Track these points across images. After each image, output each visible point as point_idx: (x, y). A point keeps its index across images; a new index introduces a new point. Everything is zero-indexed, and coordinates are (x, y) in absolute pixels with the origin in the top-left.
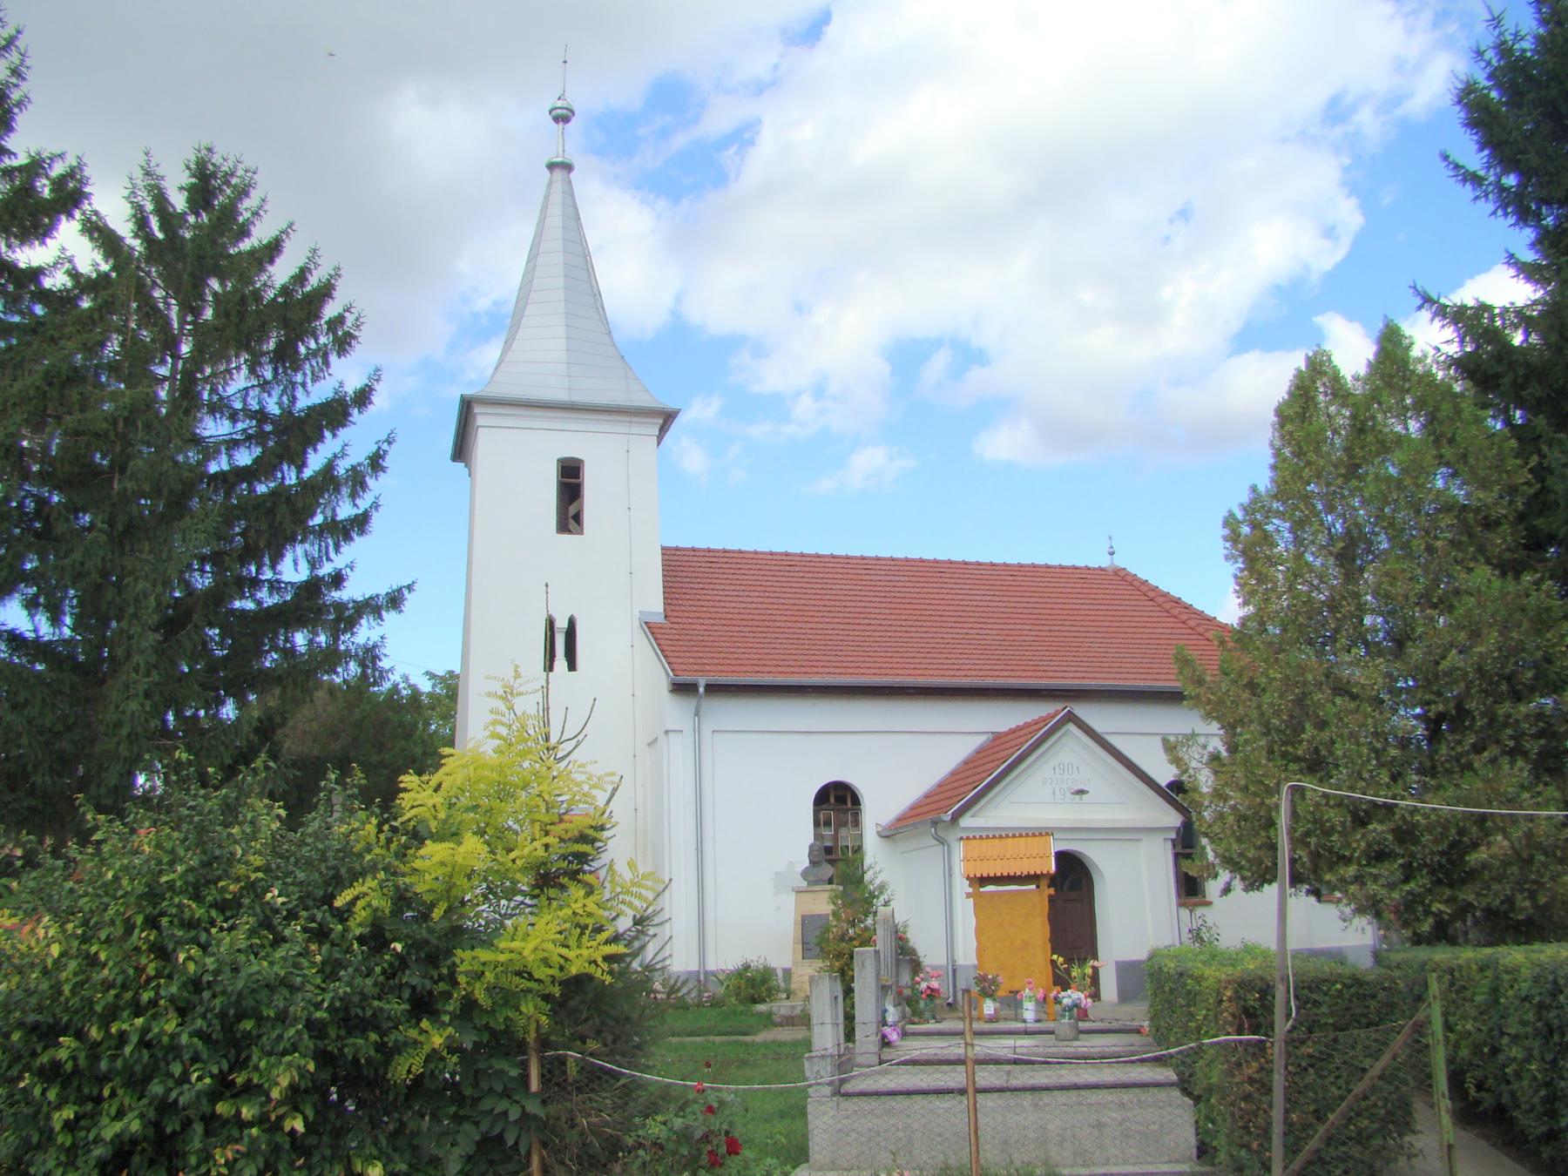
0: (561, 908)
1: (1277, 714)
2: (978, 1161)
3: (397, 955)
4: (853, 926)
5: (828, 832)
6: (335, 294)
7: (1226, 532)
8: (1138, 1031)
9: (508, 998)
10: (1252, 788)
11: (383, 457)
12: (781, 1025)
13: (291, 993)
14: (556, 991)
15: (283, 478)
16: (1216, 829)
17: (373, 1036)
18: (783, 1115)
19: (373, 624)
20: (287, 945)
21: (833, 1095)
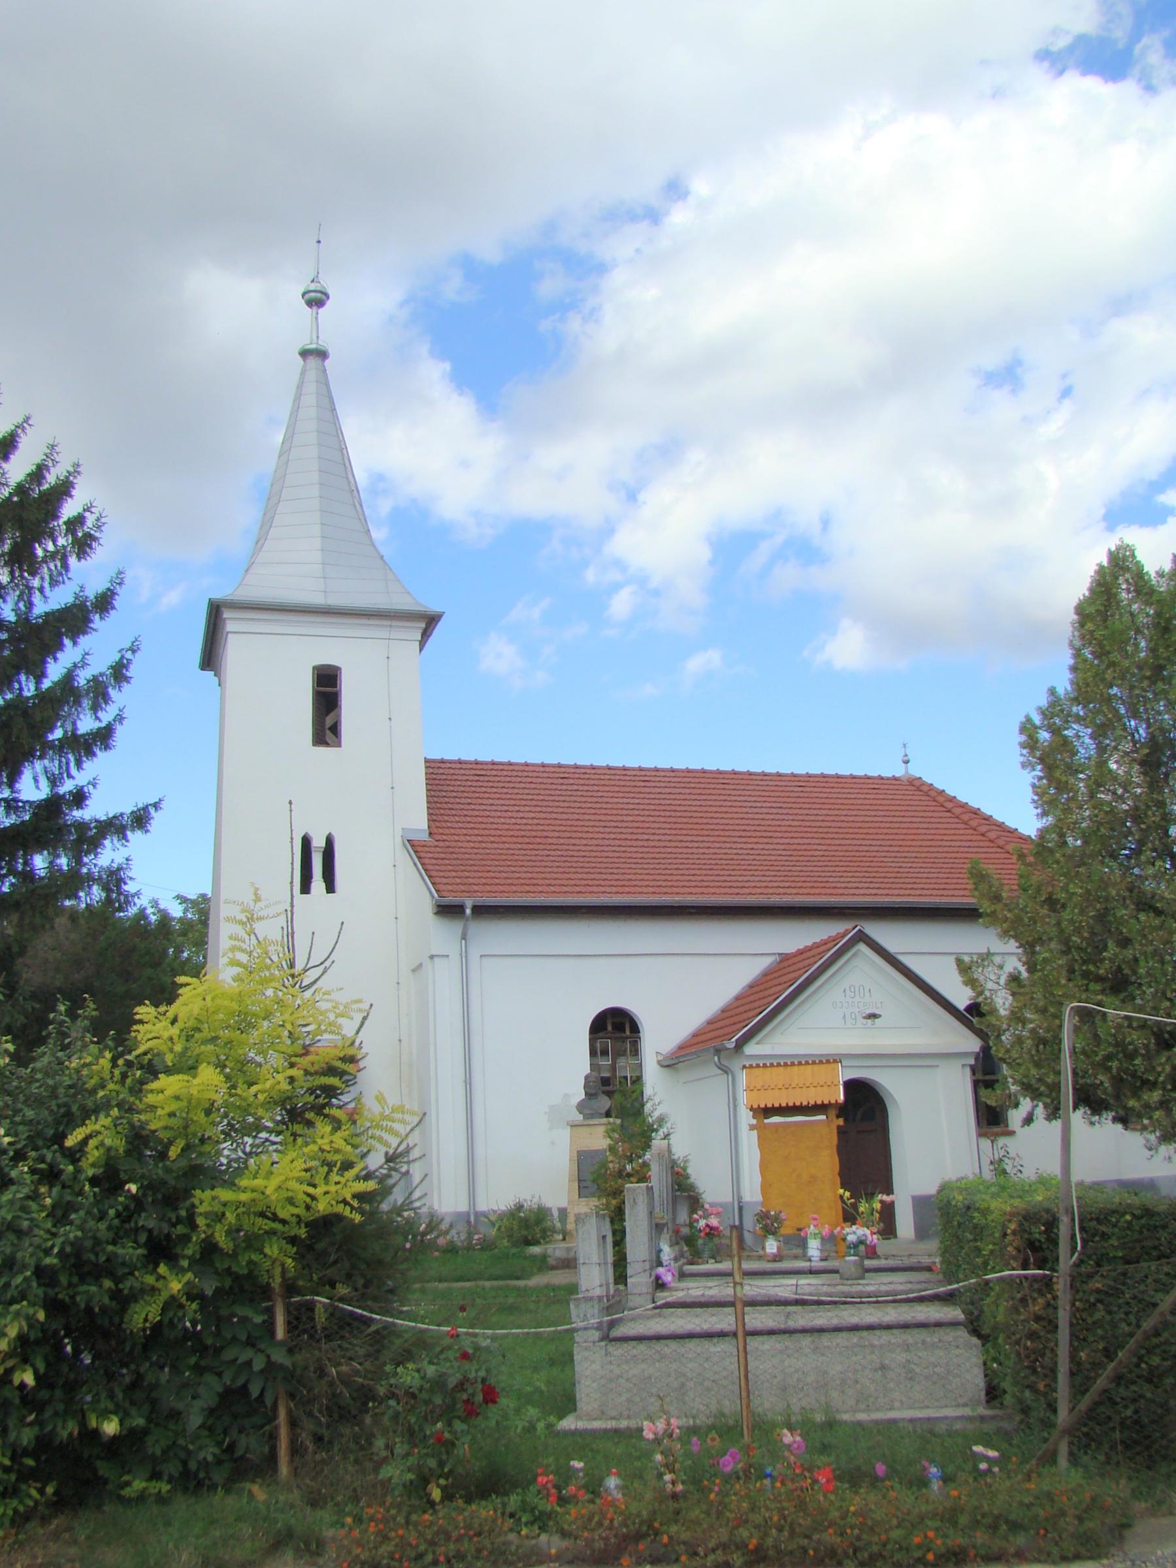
0: (307, 1144)
1: (1078, 930)
2: (748, 1406)
3: (134, 1197)
4: (631, 1161)
5: (606, 1062)
6: (74, 493)
7: (1023, 738)
8: (929, 1269)
9: (253, 1242)
10: (1052, 1010)
11: (126, 667)
12: (553, 1268)
13: (19, 1238)
14: (302, 1232)
15: (21, 689)
16: (1014, 1055)
17: (108, 1283)
18: (552, 1362)
19: (118, 845)
20: (13, 1188)
21: (601, 1340)
